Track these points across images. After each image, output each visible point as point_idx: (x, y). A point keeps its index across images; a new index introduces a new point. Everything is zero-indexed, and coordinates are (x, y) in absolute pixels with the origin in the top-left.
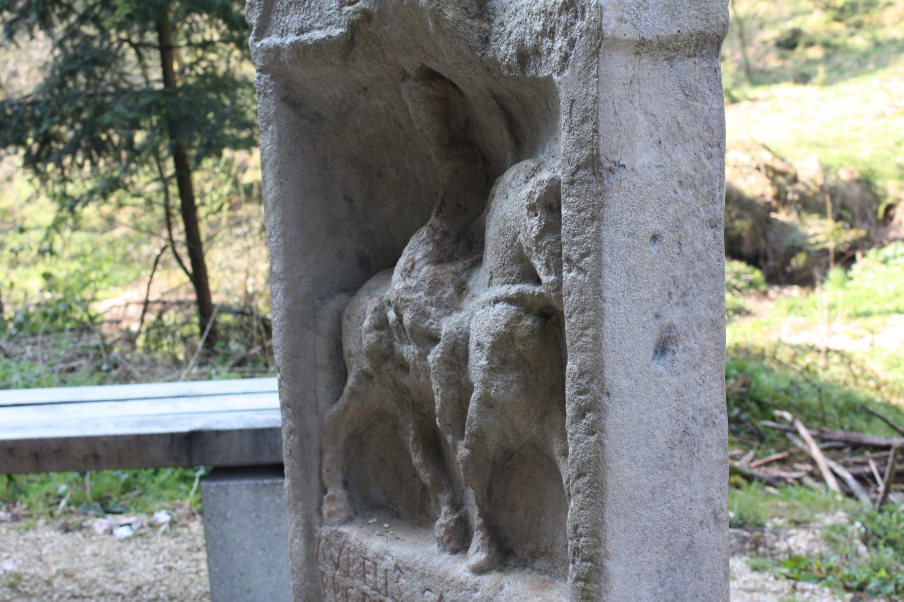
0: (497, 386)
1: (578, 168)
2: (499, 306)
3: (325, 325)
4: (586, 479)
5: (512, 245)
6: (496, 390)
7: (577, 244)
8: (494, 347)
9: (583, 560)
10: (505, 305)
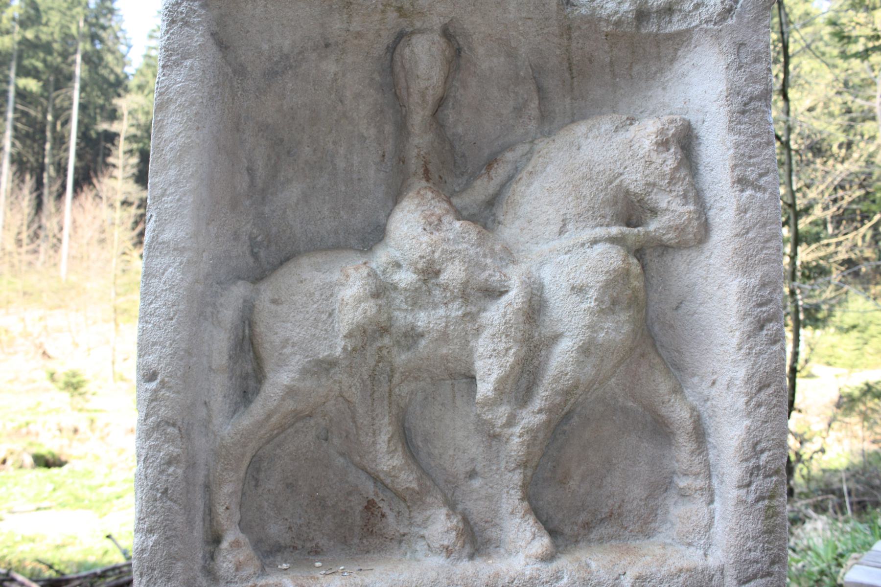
0: (608, 328)
1: (751, 99)
2: (600, 248)
3: (229, 315)
4: (770, 390)
5: (606, 188)
6: (607, 333)
7: (754, 165)
8: (607, 285)
9: (765, 477)
10: (608, 245)
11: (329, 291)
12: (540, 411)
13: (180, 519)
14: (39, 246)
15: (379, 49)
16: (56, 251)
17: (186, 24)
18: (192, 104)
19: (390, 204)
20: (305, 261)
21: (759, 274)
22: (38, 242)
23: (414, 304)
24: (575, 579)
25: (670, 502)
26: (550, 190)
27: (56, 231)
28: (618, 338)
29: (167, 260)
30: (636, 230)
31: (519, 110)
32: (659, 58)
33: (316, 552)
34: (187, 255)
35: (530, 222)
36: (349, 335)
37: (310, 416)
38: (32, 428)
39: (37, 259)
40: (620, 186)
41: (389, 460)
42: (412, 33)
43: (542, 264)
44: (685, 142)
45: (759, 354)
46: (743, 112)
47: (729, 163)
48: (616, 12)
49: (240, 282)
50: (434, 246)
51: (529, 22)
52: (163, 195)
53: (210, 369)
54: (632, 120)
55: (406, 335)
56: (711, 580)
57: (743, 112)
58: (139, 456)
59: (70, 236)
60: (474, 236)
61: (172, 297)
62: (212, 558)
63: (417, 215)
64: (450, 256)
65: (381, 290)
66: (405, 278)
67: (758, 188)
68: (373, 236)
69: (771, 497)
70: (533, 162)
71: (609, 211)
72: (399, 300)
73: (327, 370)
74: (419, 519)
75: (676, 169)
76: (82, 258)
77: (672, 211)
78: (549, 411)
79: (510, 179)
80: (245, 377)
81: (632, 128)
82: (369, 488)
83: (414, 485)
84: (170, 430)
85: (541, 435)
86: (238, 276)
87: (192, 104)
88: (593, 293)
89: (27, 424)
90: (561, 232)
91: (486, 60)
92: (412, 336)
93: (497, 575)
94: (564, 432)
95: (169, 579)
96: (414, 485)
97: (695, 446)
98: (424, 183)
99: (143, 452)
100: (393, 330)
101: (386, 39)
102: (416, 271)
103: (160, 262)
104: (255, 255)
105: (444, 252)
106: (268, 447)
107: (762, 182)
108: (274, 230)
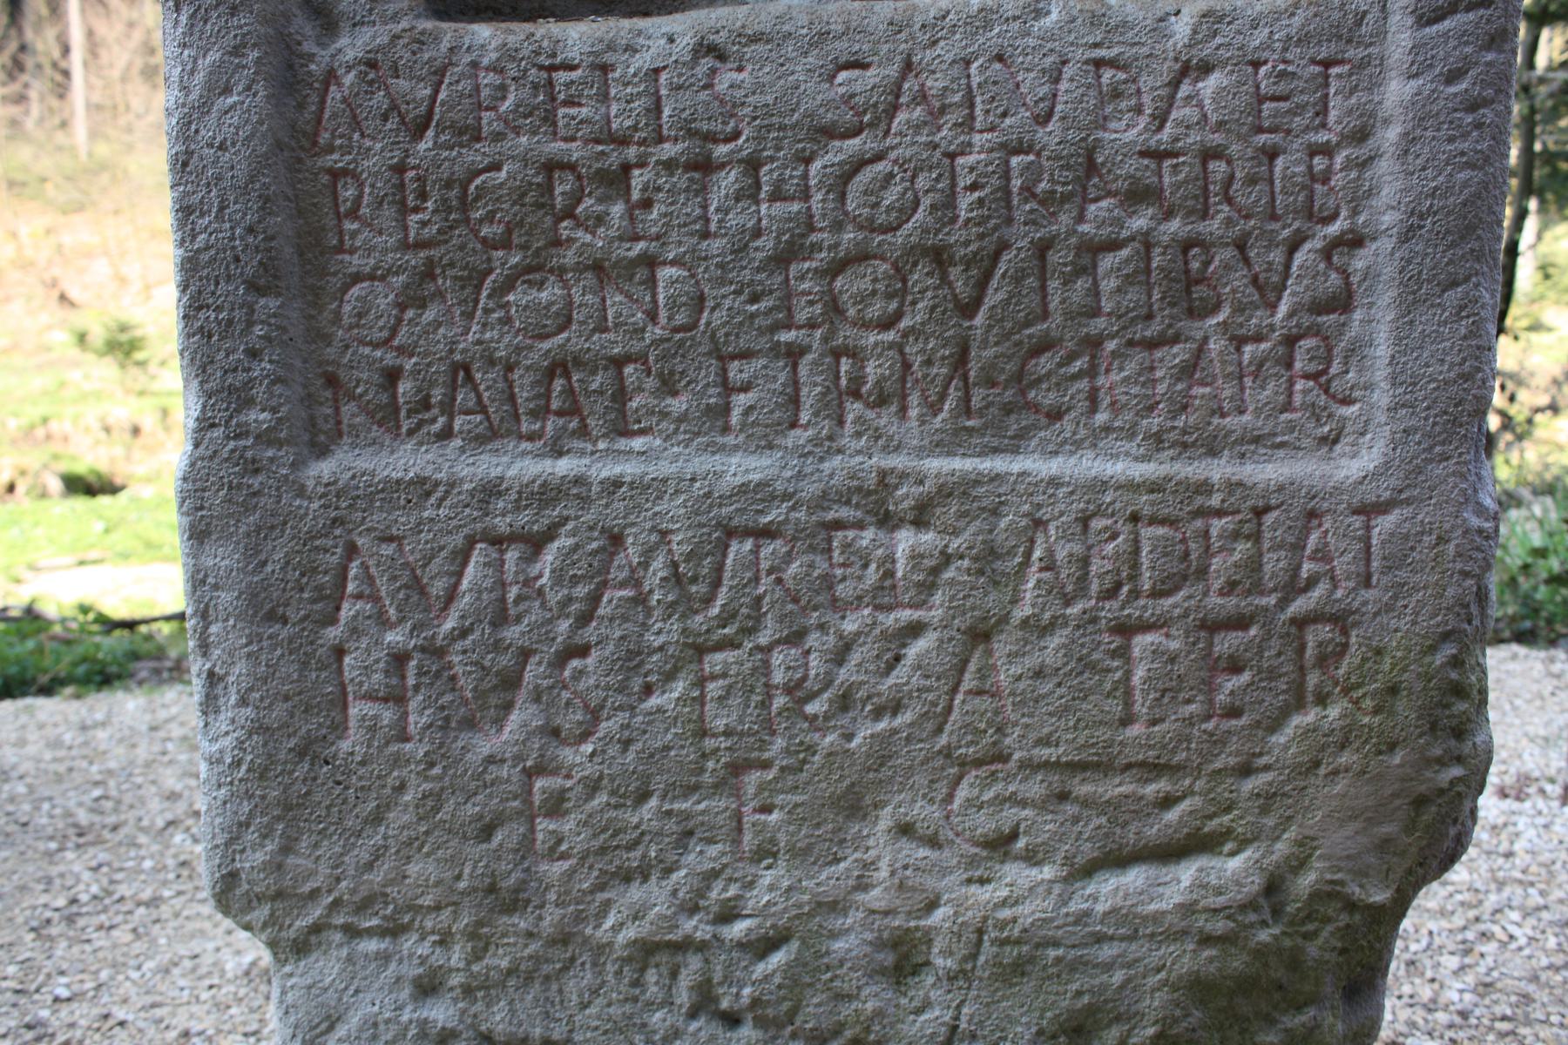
14: (26, 86)
16: (61, 97)
22: (25, 78)
24: (1075, 12)
27: (56, 54)
38: (54, 426)
39: (27, 113)
56: (1359, 23)
59: (85, 64)
76: (115, 107)
89: (45, 420)
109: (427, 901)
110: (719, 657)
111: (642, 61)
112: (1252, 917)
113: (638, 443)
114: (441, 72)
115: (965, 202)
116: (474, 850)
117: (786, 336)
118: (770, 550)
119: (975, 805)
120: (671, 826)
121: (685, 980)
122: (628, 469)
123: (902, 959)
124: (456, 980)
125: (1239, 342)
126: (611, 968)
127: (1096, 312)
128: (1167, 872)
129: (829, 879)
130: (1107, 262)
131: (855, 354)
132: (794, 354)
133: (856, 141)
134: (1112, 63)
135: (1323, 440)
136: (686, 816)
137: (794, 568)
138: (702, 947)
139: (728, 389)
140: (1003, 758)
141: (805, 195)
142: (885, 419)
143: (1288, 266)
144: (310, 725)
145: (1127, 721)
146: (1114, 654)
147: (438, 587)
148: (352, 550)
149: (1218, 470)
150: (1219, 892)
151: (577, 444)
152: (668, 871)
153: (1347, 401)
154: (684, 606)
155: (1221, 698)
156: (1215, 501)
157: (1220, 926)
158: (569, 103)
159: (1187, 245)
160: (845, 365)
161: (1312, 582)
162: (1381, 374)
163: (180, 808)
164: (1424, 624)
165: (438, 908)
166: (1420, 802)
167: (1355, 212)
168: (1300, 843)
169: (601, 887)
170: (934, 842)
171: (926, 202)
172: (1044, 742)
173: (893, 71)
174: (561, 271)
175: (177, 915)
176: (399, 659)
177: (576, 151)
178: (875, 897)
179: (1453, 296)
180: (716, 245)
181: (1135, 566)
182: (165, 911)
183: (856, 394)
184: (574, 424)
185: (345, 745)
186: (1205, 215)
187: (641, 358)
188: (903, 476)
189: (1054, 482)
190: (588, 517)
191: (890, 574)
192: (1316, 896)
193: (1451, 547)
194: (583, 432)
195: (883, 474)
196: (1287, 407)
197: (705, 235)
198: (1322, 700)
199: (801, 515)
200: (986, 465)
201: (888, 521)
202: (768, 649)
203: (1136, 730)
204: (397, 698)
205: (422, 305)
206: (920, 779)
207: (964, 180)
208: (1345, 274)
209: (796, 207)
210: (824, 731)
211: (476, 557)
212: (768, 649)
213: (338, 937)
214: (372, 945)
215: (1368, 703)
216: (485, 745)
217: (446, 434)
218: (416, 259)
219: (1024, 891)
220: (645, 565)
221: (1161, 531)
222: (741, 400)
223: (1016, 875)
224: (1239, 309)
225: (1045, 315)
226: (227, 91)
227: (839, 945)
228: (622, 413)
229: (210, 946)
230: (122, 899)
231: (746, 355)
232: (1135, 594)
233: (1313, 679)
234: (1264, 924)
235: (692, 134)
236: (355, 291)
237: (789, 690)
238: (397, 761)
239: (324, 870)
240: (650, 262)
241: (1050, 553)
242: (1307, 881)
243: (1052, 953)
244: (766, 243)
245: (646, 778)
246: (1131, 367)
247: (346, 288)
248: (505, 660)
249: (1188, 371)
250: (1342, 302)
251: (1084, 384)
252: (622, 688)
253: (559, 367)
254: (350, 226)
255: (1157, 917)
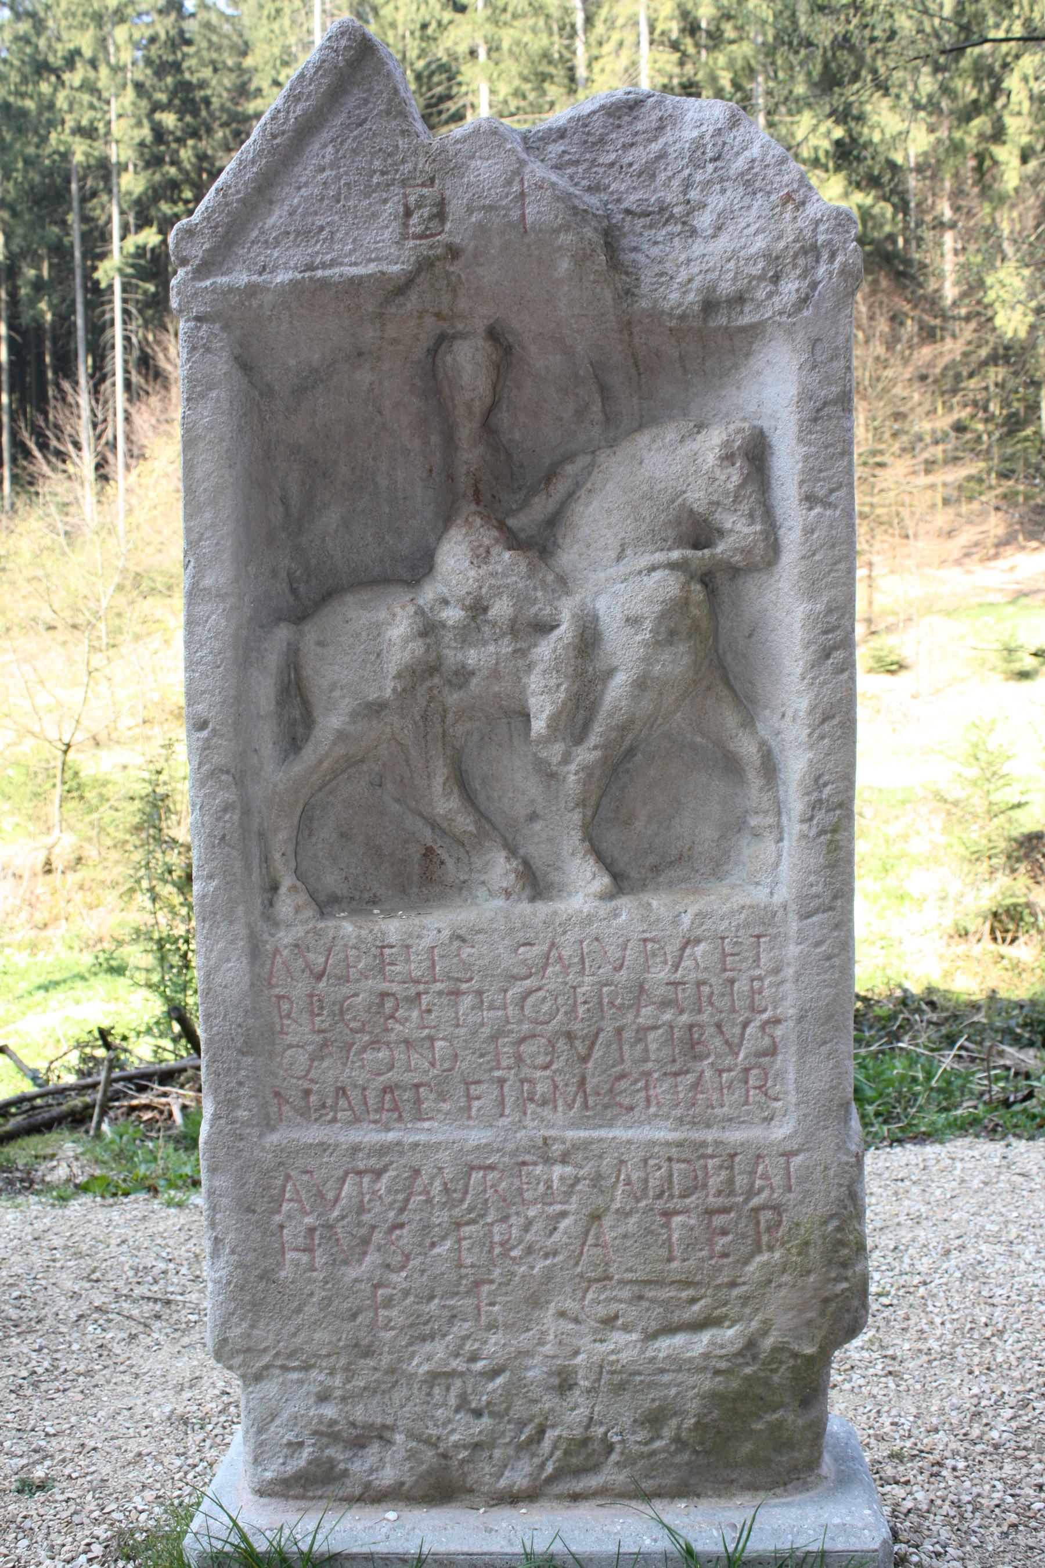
2: (657, 575)
3: (273, 659)
4: (835, 722)
8: (662, 616)
11: (376, 630)
12: (595, 748)
13: (238, 865)
15: (419, 352)
17: (208, 350)
18: (222, 440)
19: (441, 525)
20: (349, 599)
21: (825, 599)
23: (464, 641)
25: (743, 843)
26: (609, 512)
28: (677, 671)
29: (209, 607)
30: (700, 553)
31: (581, 413)
32: (733, 352)
33: (374, 901)
34: (230, 601)
35: (588, 546)
36: (399, 676)
37: (362, 761)
40: (682, 505)
41: (445, 804)
42: (454, 337)
43: (597, 594)
44: (755, 454)
45: (822, 684)
46: (815, 420)
47: (797, 478)
48: (680, 305)
49: (282, 625)
50: (480, 581)
51: (584, 320)
52: (200, 539)
53: (259, 715)
54: (700, 427)
55: (456, 673)
57: (815, 420)
58: (194, 805)
60: (523, 568)
61: (217, 645)
62: (271, 904)
63: (464, 547)
64: (497, 592)
65: (429, 629)
66: (453, 615)
67: (827, 505)
68: (419, 567)
69: (834, 831)
70: (592, 478)
71: (671, 533)
72: (448, 637)
73: (378, 712)
74: (478, 863)
75: (742, 486)
77: (738, 530)
78: (605, 747)
79: (571, 496)
80: (293, 723)
81: (699, 437)
82: (428, 836)
83: (471, 828)
84: (224, 777)
85: (597, 772)
86: (279, 618)
87: (222, 440)
88: (648, 624)
90: (619, 558)
91: (542, 360)
92: (463, 675)
93: (555, 913)
94: (627, 771)
95: (231, 923)
96: (471, 828)
97: (763, 782)
98: (473, 507)
99: (198, 801)
100: (443, 669)
101: (426, 341)
102: (464, 608)
103: (202, 610)
104: (294, 591)
105: (490, 587)
106: (321, 794)
107: (832, 498)
108: (313, 562)
109: (324, 1352)
110: (467, 1229)
111: (426, 942)
112: (741, 1360)
113: (427, 1125)
114: (330, 950)
115: (581, 1010)
116: (348, 1326)
117: (497, 1074)
118: (492, 1176)
119: (596, 1303)
120: (446, 1313)
121: (454, 1391)
122: (422, 1138)
123: (564, 1383)
124: (338, 1393)
125: (720, 1072)
126: (416, 1386)
127: (646, 1060)
128: (695, 1338)
129: (524, 1340)
130: (652, 1036)
131: (531, 1082)
132: (501, 1082)
133: (528, 982)
134: (652, 940)
135: (765, 1119)
136: (453, 1307)
137: (503, 1185)
138: (462, 1374)
139: (469, 1098)
140: (609, 1278)
141: (504, 1007)
142: (546, 1112)
143: (743, 1034)
144: (265, 1264)
145: (670, 1260)
146: (662, 1226)
147: (330, 1196)
148: (288, 1177)
149: (710, 1135)
150: (722, 1347)
151: (398, 1125)
152: (444, 1335)
153: (776, 1099)
154: (450, 1204)
155: (718, 1248)
156: (710, 1151)
157: (723, 1365)
158: (391, 964)
159: (691, 1027)
160: (526, 1086)
161: (761, 1190)
162: (791, 1087)
163: (83, 1307)
164: (820, 1211)
165: (329, 1356)
166: (826, 1301)
167: (775, 1008)
168: (764, 1322)
169: (411, 1344)
170: (576, 1321)
171: (562, 1010)
172: (630, 1270)
173: (545, 947)
174: (388, 1044)
175: (108, 1382)
176: (312, 1230)
177: (395, 988)
178: (548, 1349)
179: (824, 1049)
180: (462, 1031)
181: (671, 1182)
182: (98, 1378)
183: (532, 1100)
184: (396, 1115)
185: (283, 1274)
186: (700, 1011)
187: (427, 1084)
188: (555, 1139)
189: (629, 1142)
190: (403, 1162)
191: (550, 1187)
192: (776, 1349)
193: (832, 1172)
194: (400, 1118)
195: (545, 1139)
196: (746, 1103)
197: (457, 1026)
198: (771, 1248)
199: (506, 1159)
200: (596, 1134)
201: (548, 1161)
202: (492, 1224)
203: (675, 1264)
204: (309, 1250)
205: (322, 1059)
206: (568, 1289)
207: (580, 1000)
208: (772, 1037)
209: (500, 1013)
210: (520, 1265)
211: (349, 1181)
212: (492, 1224)
213: (277, 1371)
214: (295, 1376)
215: (794, 1251)
216: (352, 1273)
217: (334, 1120)
218: (318, 1038)
219: (623, 1346)
220: (431, 1184)
221: (683, 1166)
222: (476, 1104)
223: (618, 1338)
224: (718, 1056)
225: (623, 1061)
226: (228, 960)
227: (530, 1374)
228: (419, 1110)
229: (139, 1402)
230: (65, 1371)
231: (479, 1082)
232: (672, 1196)
233: (765, 1238)
234: (747, 1364)
235: (450, 978)
236: (289, 1052)
237: (502, 1244)
238: (310, 1281)
239: (271, 1336)
240: (431, 1039)
241: (628, 1176)
242: (768, 1343)
243: (638, 1378)
244: (486, 1031)
245: (433, 1289)
246: (665, 1086)
247: (284, 1051)
248: (363, 1231)
249: (696, 1085)
250: (772, 1051)
251: (643, 1094)
252: (420, 1244)
253: (388, 1089)
254: (286, 1022)
255: (691, 1360)
